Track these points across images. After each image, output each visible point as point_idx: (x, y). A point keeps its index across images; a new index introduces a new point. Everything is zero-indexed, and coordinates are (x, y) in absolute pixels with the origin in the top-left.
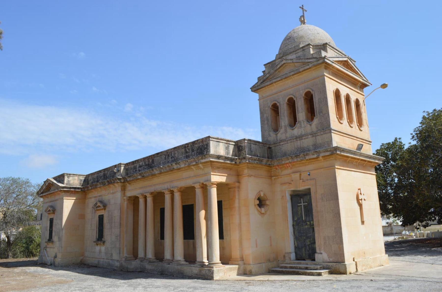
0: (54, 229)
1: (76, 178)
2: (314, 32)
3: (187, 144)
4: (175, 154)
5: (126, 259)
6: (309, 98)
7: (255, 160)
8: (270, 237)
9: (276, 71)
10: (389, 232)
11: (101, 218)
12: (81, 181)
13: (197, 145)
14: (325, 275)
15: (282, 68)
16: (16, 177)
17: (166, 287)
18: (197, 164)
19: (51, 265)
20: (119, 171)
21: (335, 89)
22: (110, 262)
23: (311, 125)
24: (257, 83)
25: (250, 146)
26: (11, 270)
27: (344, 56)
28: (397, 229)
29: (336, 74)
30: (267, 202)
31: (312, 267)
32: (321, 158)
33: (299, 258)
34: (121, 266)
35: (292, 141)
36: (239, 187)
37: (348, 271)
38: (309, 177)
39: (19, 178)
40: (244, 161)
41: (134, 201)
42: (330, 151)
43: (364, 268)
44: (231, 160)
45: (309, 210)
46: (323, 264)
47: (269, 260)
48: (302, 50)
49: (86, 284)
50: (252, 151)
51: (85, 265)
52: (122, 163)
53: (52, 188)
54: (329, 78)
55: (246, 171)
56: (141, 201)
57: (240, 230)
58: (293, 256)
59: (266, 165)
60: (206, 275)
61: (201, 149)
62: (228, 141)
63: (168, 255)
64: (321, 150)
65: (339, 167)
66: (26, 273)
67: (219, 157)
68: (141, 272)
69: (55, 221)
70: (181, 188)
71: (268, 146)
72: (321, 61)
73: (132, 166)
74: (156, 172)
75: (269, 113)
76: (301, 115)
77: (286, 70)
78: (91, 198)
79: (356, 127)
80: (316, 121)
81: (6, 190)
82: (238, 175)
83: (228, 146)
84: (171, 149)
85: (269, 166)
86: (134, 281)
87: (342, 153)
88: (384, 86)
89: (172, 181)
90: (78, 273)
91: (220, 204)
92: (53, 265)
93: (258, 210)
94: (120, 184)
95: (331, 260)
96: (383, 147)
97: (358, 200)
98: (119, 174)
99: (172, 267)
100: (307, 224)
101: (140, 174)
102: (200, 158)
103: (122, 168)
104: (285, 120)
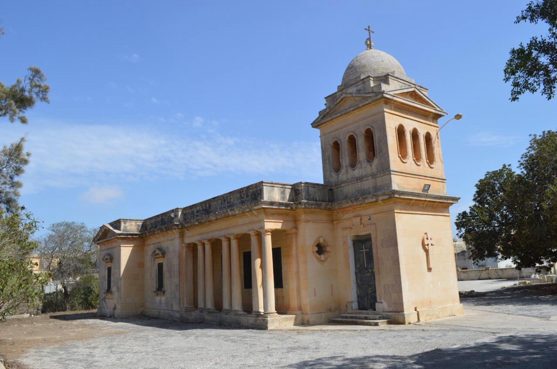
0: (112, 279)
1: (133, 223)
2: (380, 59)
3: (241, 189)
4: (230, 198)
5: (187, 310)
6: (369, 135)
7: (312, 205)
8: (332, 286)
9: (336, 105)
10: (487, 277)
11: (160, 266)
12: (139, 226)
13: (251, 191)
14: (383, 325)
15: (341, 103)
16: (70, 221)
17: (217, 336)
18: (251, 211)
19: (111, 317)
20: (176, 216)
21: (397, 125)
22: (171, 313)
23: (371, 166)
24: (318, 118)
25: (308, 189)
26: (69, 322)
27: (413, 86)
28: (527, 271)
29: (399, 108)
30: (328, 249)
31: (371, 316)
32: (380, 202)
33: (362, 307)
34: (182, 317)
35: (353, 182)
36: (296, 234)
37: (407, 321)
38: (369, 222)
39: (73, 223)
40: (299, 206)
41: (193, 248)
42: (388, 194)
43: (428, 318)
44: (286, 205)
45: (370, 256)
46: (384, 313)
47: (330, 310)
48: (362, 82)
49: (142, 334)
50: (309, 195)
51: (146, 316)
52: (179, 207)
53: (109, 235)
54: (390, 113)
55: (303, 217)
56: (200, 248)
57: (298, 280)
58: (355, 305)
59: (325, 209)
60: (260, 324)
61: (255, 195)
62: (284, 185)
63: (226, 306)
64: (379, 193)
65: (399, 211)
66: (84, 325)
67: (272, 203)
68: (200, 323)
69: (112, 270)
70: (237, 235)
71: (329, 188)
72: (379, 96)
73: (190, 211)
74: (212, 218)
75: (330, 150)
76: (362, 155)
77: (347, 105)
78: (149, 245)
79: (424, 165)
80: (376, 161)
81: (60, 237)
82: (296, 221)
83: (284, 190)
84: (227, 194)
85: (330, 209)
86: (189, 331)
87: (401, 197)
88: (458, 117)
89: (228, 228)
90: (137, 324)
91: (277, 253)
92: (112, 318)
93: (316, 257)
94: (177, 230)
95: (391, 309)
96: (488, 176)
97: (423, 245)
98: (176, 219)
99: (230, 317)
100: (368, 272)
101: (197, 220)
102: (253, 204)
103: (180, 213)
104: (345, 160)
